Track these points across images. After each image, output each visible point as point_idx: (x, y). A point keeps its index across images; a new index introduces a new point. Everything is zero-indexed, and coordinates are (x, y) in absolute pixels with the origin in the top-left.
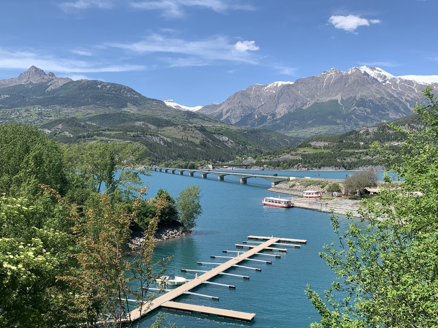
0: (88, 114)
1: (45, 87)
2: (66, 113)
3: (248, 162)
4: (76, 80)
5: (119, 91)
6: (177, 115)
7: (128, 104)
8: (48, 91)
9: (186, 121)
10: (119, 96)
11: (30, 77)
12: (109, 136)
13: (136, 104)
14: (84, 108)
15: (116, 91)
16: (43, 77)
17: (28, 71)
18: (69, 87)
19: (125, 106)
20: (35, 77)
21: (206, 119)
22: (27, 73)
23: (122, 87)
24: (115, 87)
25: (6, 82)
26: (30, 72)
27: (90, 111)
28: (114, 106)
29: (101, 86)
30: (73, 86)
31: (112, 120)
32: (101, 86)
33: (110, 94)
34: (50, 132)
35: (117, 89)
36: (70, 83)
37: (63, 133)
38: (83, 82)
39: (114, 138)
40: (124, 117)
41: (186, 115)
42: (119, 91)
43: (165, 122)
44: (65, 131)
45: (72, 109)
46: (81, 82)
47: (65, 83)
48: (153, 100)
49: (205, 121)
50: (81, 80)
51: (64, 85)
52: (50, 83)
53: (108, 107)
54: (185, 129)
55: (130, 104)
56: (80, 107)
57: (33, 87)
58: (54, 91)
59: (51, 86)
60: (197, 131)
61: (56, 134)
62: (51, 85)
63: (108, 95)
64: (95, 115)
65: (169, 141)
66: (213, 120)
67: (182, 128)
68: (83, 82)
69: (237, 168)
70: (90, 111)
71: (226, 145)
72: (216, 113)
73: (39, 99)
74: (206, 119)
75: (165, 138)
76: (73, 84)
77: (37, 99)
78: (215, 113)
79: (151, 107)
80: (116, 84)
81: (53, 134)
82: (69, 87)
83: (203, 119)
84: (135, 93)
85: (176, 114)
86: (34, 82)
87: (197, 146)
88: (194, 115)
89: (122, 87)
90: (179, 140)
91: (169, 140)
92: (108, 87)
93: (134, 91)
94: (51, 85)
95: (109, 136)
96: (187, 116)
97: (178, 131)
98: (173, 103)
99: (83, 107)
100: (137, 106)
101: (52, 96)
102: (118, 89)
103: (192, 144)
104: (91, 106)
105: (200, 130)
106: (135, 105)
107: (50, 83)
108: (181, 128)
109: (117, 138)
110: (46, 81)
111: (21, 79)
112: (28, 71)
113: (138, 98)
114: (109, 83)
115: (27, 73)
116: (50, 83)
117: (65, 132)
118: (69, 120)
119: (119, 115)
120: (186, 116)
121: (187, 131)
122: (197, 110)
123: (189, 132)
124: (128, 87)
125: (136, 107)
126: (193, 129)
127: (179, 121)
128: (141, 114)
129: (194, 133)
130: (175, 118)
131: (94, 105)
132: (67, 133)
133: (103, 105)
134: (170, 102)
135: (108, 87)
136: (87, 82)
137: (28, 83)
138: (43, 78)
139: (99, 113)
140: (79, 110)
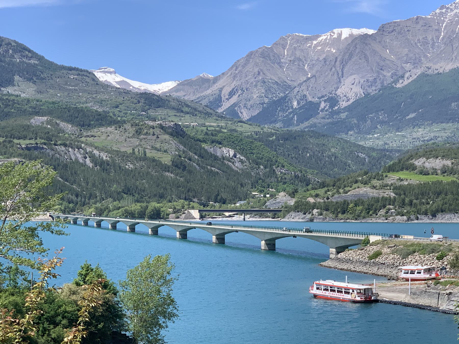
3: (279, 203)
7: (17, 78)
9: (142, 115)
13: (32, 79)
41: (143, 101)
43: (96, 117)
48: (71, 69)
49: (182, 114)
54: (138, 132)
55: (21, 79)
60: (167, 137)
65: (105, 158)
66: (200, 112)
67: (132, 130)
69: (253, 217)
71: (229, 167)
75: (96, 152)
78: (205, 97)
79: (66, 84)
84: (30, 55)
85: (120, 99)
87: (166, 168)
88: (158, 101)
89: (3, 41)
91: (104, 156)
93: (30, 51)
96: (144, 103)
98: (113, 76)
100: (34, 83)
106: (30, 80)
121: (145, 137)
123: (149, 137)
126: (157, 131)
129: (159, 140)
130: (117, 107)
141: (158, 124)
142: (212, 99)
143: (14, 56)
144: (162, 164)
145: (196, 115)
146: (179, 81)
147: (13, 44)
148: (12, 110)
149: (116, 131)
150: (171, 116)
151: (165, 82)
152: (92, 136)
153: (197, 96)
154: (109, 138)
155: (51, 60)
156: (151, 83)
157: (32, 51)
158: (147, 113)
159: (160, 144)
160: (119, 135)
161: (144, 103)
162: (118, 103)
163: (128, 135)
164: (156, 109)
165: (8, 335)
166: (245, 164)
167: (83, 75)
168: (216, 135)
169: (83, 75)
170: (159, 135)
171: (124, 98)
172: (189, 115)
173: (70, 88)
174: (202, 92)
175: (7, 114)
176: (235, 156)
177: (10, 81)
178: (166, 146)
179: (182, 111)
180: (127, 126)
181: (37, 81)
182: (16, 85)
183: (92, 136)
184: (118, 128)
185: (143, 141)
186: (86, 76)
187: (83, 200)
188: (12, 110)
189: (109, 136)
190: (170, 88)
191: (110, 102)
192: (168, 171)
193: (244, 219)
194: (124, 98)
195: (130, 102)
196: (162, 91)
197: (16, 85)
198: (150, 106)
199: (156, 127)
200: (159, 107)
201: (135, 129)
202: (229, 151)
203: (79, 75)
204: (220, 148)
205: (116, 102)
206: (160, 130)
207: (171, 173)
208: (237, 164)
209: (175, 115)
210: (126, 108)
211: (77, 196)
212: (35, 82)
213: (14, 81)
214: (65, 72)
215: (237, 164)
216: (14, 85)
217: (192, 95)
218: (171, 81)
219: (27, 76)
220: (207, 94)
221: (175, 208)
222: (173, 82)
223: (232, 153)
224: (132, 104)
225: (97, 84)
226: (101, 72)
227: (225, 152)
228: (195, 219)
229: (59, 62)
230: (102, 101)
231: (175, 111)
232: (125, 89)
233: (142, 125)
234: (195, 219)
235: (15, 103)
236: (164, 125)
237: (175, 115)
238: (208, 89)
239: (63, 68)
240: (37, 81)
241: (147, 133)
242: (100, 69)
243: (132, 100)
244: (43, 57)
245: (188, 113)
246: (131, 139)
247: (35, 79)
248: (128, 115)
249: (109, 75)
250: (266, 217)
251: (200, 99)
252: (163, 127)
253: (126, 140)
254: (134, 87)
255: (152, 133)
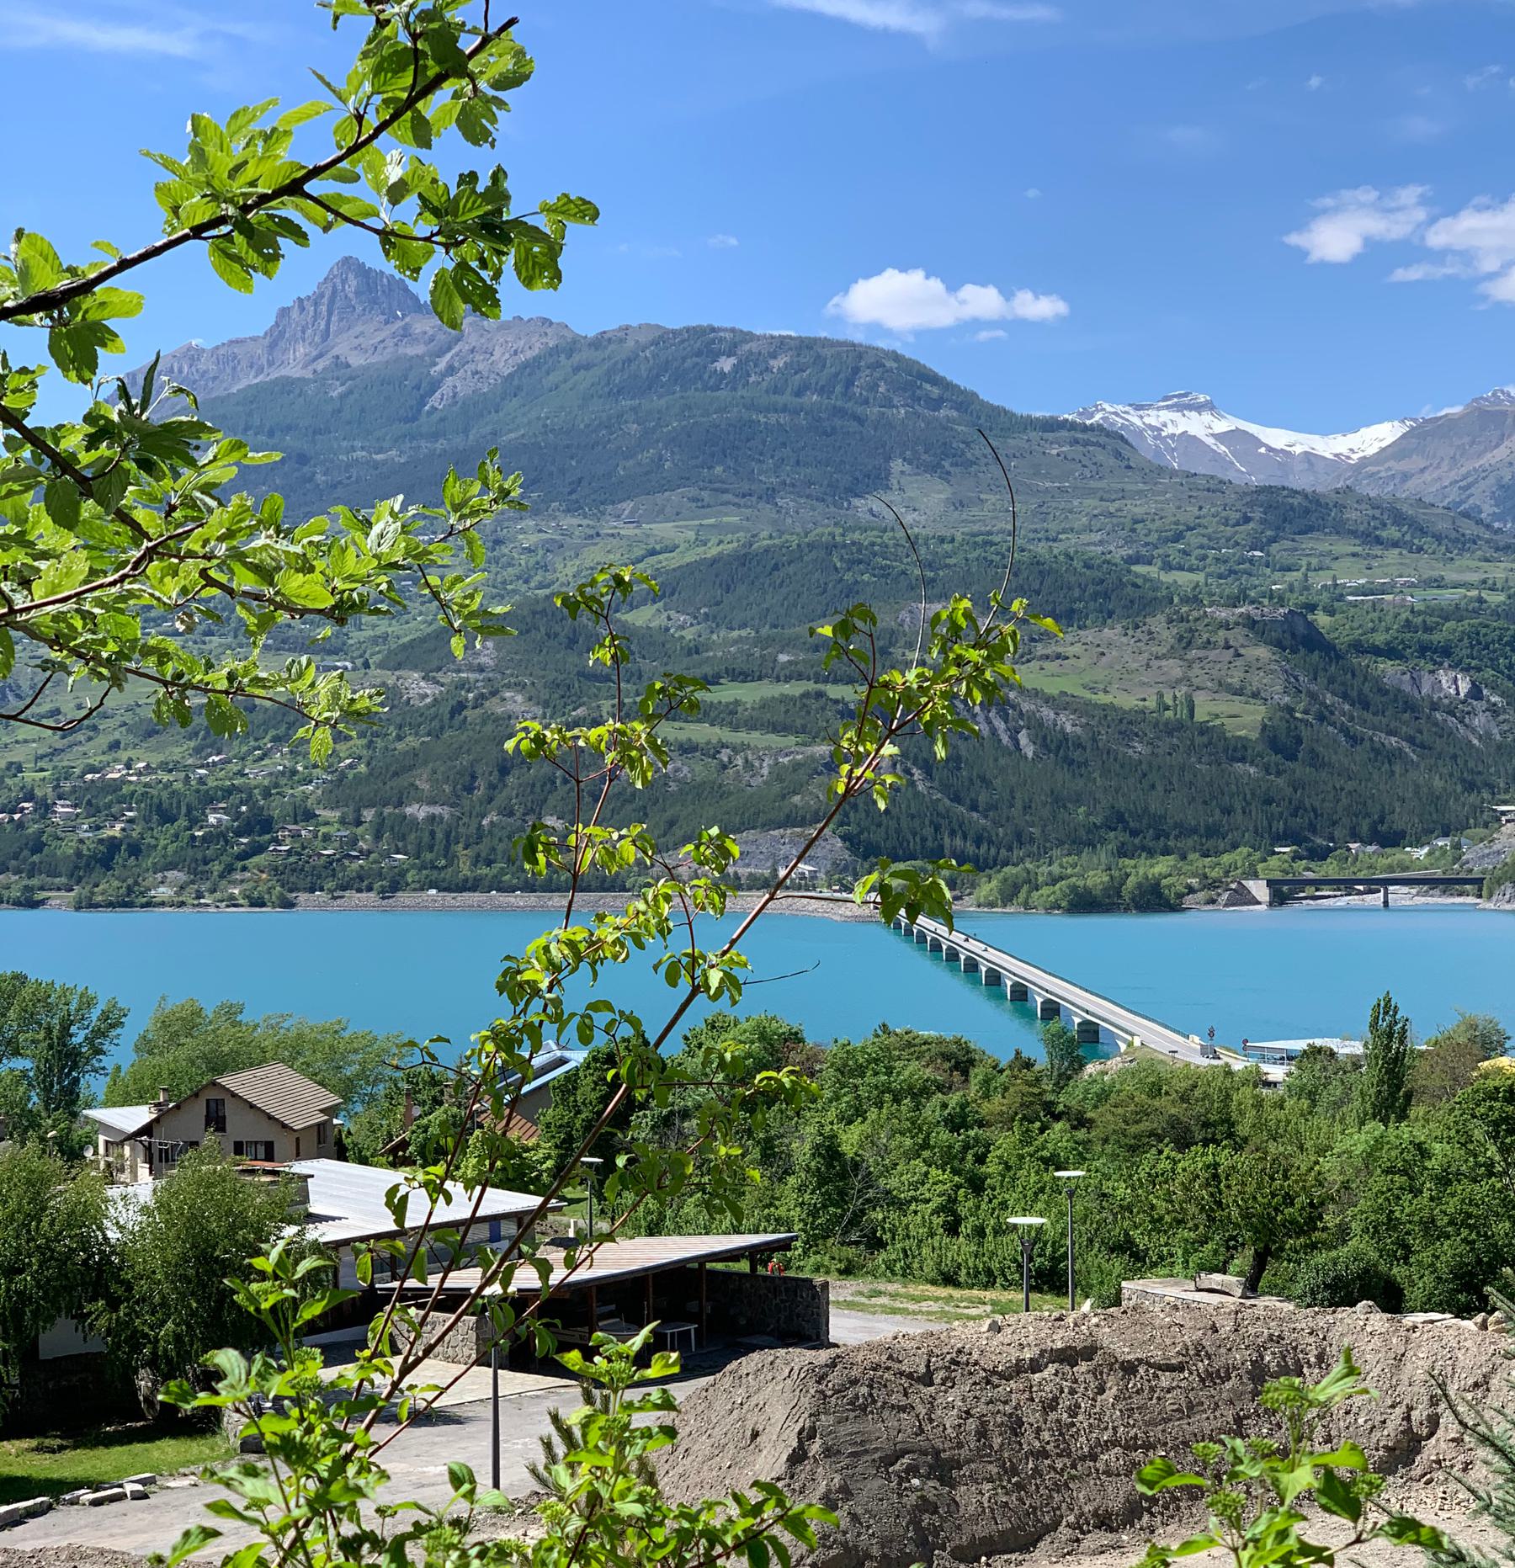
0: (653, 553)
1: (417, 387)
2: (529, 550)
3: (1499, 853)
4: (591, 334)
5: (839, 389)
6: (1192, 522)
7: (897, 465)
8: (434, 409)
9: (1251, 561)
10: (838, 422)
11: (333, 328)
12: (729, 715)
13: (939, 465)
14: (633, 512)
15: (821, 391)
16: (406, 328)
17: (322, 295)
18: (554, 378)
19: (876, 480)
20: (358, 329)
21: (1392, 532)
22: (316, 304)
23: (860, 356)
24: (820, 361)
25: (202, 367)
26: (332, 302)
27: (663, 530)
28: (810, 484)
29: (733, 360)
30: (576, 370)
31: (784, 590)
32: (733, 360)
33: (785, 409)
34: (430, 690)
35: (830, 370)
36: (555, 351)
37: (495, 700)
38: (630, 343)
39: (751, 725)
40: (852, 563)
41: (1257, 514)
42: (839, 389)
43: (1091, 589)
44: (508, 686)
45: (568, 522)
46: (622, 341)
47: (529, 354)
48: (1051, 426)
49: (1377, 551)
50: (620, 329)
51: (524, 366)
52: (442, 364)
53: (770, 495)
54: (1186, 642)
55: (907, 468)
56: (610, 508)
57: (350, 392)
58: (470, 410)
59: (449, 381)
60: (1263, 652)
61: (461, 706)
62: (451, 370)
63: (773, 418)
64: (690, 557)
65: (1069, 728)
66: (1438, 538)
67: (1167, 635)
68: (630, 343)
69: (1426, 894)
70: (663, 530)
71: (1443, 732)
72: (1494, 468)
73: (385, 462)
74: (1392, 532)
75: (1047, 713)
76: (577, 358)
77: (376, 465)
78: (1485, 472)
79: (1036, 474)
80: (826, 343)
81: (445, 710)
82: (554, 378)
83: (1371, 538)
84: (935, 392)
85: (1190, 513)
86: (356, 360)
87: (1238, 751)
88: (1307, 511)
89: (860, 356)
90: (1128, 724)
91: (1068, 724)
92: (777, 364)
93: (935, 380)
94: (451, 370)
95: (729, 715)
96: (1263, 522)
97: (1146, 655)
98: (1207, 417)
99: (628, 506)
100: (946, 476)
101: (459, 441)
102: (837, 374)
103: (1205, 739)
104: (674, 496)
105: (1279, 645)
106: (933, 468)
107: (448, 356)
108: (1166, 634)
109: (776, 728)
110: (419, 349)
111: (282, 344)
112: (322, 295)
113: (954, 421)
114: (782, 341)
115: (316, 304)
116: (442, 364)
117: (508, 695)
118: (534, 613)
119: (822, 554)
120: (1251, 525)
121: (1201, 653)
122: (1371, 450)
123: (1213, 654)
124: (896, 357)
125: (939, 484)
126: (1237, 636)
127: (1204, 558)
128: (959, 537)
129: (1239, 662)
130: (1178, 537)
131: (693, 491)
132: (519, 698)
133: (746, 487)
134: (1190, 407)
135: (777, 364)
136: (655, 343)
137: (320, 365)
138: (406, 333)
139: (714, 540)
140: (609, 526)
141: (1241, 615)
142: (1507, 478)
143: (891, 400)
144: (1226, 739)
145: (1420, 549)
146: (1414, 420)
147: (890, 364)
148: (866, 577)
149: (1124, 640)
150: (1342, 556)
151: (1367, 425)
152: (1058, 656)
153: (1463, 471)
154: (1104, 659)
155: (996, 403)
156: (1325, 433)
157: (943, 379)
158: (1268, 555)
159: (1242, 675)
160: (1130, 650)
161: (1263, 522)
162: (1181, 527)
163: (1155, 649)
164: (1297, 537)
165: (501, 1201)
166: (1501, 718)
167: (1087, 443)
168: (1428, 629)
169: (1087, 443)
170: (1243, 646)
171: (1201, 508)
172: (1397, 551)
173: (1048, 485)
174: (1480, 455)
175: (851, 591)
176: (1475, 693)
177: (878, 477)
178: (1256, 680)
179: (1379, 541)
180: (1157, 623)
181: (952, 469)
182: (896, 486)
183: (1058, 656)
184: (1130, 632)
185: (1196, 666)
186: (1097, 444)
187: (993, 851)
188: (866, 577)
189: (1103, 654)
190: (1384, 444)
191: (1158, 523)
192: (1243, 760)
193: (1386, 903)
194: (1201, 508)
195: (1218, 523)
196: (1361, 454)
197: (896, 486)
198: (1278, 528)
199: (1237, 624)
200: (1309, 529)
201: (1175, 631)
202: (1455, 681)
203: (1077, 442)
204: (1432, 672)
205: (1177, 523)
206: (1246, 631)
207: (1252, 763)
208: (1480, 721)
209: (1354, 555)
210: (1205, 541)
211: (978, 842)
212: (948, 473)
213: (889, 473)
214: (1033, 435)
215: (1480, 721)
216: (888, 488)
217: (1445, 466)
218: (1390, 420)
219: (925, 457)
220: (1493, 462)
221: (1205, 877)
222: (1396, 423)
223: (1464, 686)
224: (1222, 528)
225: (1128, 467)
226: (1167, 407)
227: (1445, 685)
228: (1259, 903)
229: (1022, 407)
230: (1136, 522)
231: (1357, 542)
232: (1212, 477)
233: (1197, 620)
234: (1259, 903)
235: (875, 554)
236: (1258, 618)
237: (1354, 555)
238: (1497, 446)
239: (1029, 424)
240: (952, 469)
241: (1209, 642)
242: (1167, 398)
243: (1224, 514)
244: (974, 395)
245: (1395, 544)
246: (1164, 663)
247: (946, 464)
248: (1208, 561)
249: (1194, 414)
250: (1460, 895)
251: (1470, 480)
252: (1255, 622)
253: (1148, 666)
254: (1270, 449)
255: (1222, 643)
